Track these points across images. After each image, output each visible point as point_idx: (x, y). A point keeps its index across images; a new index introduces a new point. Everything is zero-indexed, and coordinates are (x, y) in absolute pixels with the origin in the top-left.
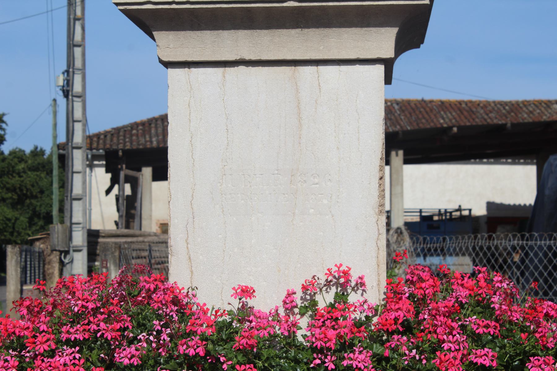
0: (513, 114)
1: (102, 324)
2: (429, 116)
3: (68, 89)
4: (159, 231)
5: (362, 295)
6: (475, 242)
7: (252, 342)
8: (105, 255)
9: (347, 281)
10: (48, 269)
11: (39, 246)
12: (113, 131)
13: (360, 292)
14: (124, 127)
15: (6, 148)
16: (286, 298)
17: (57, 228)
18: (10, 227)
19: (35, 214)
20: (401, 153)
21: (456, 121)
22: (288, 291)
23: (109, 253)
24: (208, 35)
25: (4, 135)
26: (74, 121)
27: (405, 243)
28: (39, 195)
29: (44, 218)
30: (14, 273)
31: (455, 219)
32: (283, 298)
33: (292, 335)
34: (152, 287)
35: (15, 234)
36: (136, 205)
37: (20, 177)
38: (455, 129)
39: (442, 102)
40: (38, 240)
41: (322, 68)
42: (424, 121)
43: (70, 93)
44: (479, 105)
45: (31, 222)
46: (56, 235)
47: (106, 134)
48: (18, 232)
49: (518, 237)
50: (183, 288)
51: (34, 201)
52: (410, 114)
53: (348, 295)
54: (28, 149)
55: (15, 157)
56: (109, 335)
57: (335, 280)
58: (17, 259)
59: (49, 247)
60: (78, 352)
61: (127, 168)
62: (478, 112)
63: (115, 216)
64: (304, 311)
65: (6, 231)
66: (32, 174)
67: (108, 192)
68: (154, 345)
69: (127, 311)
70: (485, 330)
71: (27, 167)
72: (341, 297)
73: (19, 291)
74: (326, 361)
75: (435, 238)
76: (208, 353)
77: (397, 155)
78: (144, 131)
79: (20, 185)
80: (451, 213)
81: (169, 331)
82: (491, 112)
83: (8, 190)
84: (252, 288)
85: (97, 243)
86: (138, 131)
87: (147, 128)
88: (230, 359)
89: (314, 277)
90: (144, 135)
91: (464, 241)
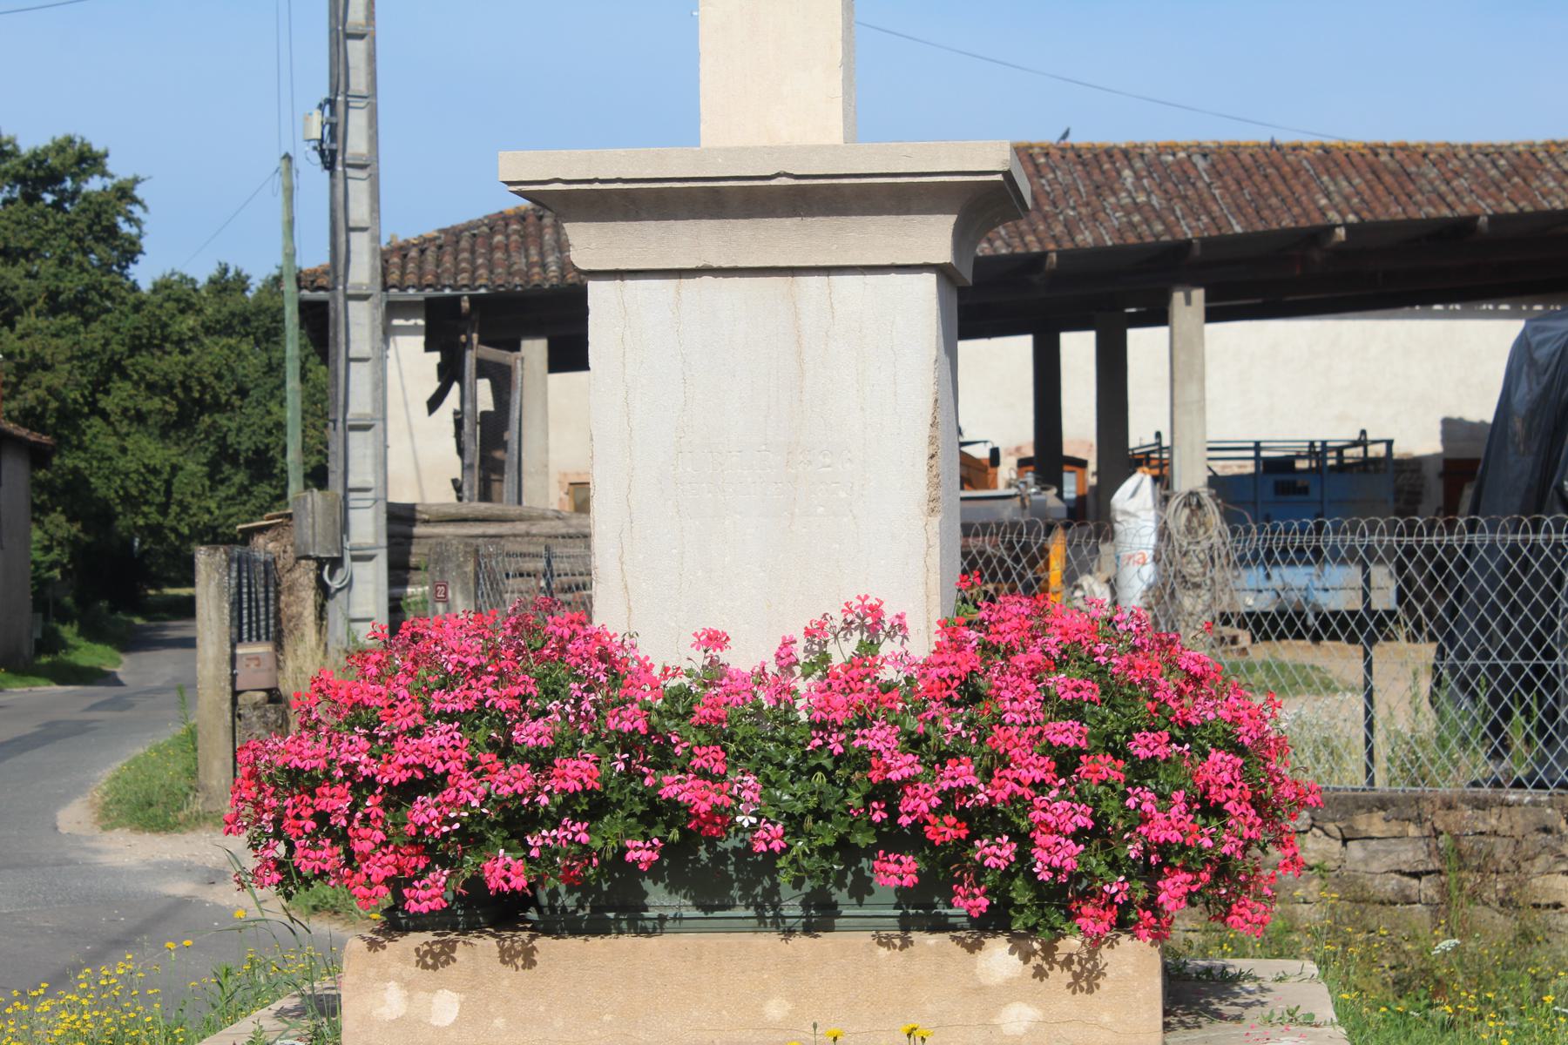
0: (1516, 179)
1: (490, 691)
2: (1290, 188)
3: (334, 146)
4: (568, 507)
5: (902, 643)
6: (1286, 540)
8: (442, 572)
9: (878, 621)
10: (287, 605)
11: (264, 546)
12: (443, 236)
13: (898, 639)
14: (470, 226)
15: (144, 274)
16: (781, 649)
17: (310, 505)
18: (157, 491)
19: (224, 455)
20: (1198, 295)
21: (1363, 200)
22: (784, 638)
24: (651, 228)
25: (140, 236)
26: (349, 230)
27: (1210, 532)
28: (236, 401)
30: (213, 615)
32: (776, 649)
34: (567, 633)
35: (174, 509)
36: (506, 436)
37: (185, 352)
38: (1341, 233)
39: (1326, 150)
40: (261, 530)
41: (836, 279)
42: (1274, 201)
43: (340, 158)
44: (1425, 155)
46: (310, 520)
47: (423, 246)
48: (180, 503)
49: (1440, 528)
50: (615, 635)
51: (221, 419)
52: (1239, 183)
53: (879, 644)
54: (202, 273)
55: (168, 298)
57: (858, 621)
58: (221, 579)
59: (289, 548)
60: (459, 730)
61: (482, 342)
62: (1424, 175)
63: (454, 467)
64: (809, 669)
65: (146, 502)
66: (217, 344)
67: (434, 403)
68: (572, 718)
70: (1074, 694)
71: (203, 325)
73: (227, 658)
74: (831, 741)
75: (1296, 525)
76: (652, 730)
77: (1188, 301)
78: (524, 236)
79: (184, 374)
80: (1340, 450)
82: (1457, 174)
84: (724, 634)
86: (508, 237)
87: (531, 229)
88: (687, 739)
89: (824, 615)
90: (524, 247)
91: (1262, 536)
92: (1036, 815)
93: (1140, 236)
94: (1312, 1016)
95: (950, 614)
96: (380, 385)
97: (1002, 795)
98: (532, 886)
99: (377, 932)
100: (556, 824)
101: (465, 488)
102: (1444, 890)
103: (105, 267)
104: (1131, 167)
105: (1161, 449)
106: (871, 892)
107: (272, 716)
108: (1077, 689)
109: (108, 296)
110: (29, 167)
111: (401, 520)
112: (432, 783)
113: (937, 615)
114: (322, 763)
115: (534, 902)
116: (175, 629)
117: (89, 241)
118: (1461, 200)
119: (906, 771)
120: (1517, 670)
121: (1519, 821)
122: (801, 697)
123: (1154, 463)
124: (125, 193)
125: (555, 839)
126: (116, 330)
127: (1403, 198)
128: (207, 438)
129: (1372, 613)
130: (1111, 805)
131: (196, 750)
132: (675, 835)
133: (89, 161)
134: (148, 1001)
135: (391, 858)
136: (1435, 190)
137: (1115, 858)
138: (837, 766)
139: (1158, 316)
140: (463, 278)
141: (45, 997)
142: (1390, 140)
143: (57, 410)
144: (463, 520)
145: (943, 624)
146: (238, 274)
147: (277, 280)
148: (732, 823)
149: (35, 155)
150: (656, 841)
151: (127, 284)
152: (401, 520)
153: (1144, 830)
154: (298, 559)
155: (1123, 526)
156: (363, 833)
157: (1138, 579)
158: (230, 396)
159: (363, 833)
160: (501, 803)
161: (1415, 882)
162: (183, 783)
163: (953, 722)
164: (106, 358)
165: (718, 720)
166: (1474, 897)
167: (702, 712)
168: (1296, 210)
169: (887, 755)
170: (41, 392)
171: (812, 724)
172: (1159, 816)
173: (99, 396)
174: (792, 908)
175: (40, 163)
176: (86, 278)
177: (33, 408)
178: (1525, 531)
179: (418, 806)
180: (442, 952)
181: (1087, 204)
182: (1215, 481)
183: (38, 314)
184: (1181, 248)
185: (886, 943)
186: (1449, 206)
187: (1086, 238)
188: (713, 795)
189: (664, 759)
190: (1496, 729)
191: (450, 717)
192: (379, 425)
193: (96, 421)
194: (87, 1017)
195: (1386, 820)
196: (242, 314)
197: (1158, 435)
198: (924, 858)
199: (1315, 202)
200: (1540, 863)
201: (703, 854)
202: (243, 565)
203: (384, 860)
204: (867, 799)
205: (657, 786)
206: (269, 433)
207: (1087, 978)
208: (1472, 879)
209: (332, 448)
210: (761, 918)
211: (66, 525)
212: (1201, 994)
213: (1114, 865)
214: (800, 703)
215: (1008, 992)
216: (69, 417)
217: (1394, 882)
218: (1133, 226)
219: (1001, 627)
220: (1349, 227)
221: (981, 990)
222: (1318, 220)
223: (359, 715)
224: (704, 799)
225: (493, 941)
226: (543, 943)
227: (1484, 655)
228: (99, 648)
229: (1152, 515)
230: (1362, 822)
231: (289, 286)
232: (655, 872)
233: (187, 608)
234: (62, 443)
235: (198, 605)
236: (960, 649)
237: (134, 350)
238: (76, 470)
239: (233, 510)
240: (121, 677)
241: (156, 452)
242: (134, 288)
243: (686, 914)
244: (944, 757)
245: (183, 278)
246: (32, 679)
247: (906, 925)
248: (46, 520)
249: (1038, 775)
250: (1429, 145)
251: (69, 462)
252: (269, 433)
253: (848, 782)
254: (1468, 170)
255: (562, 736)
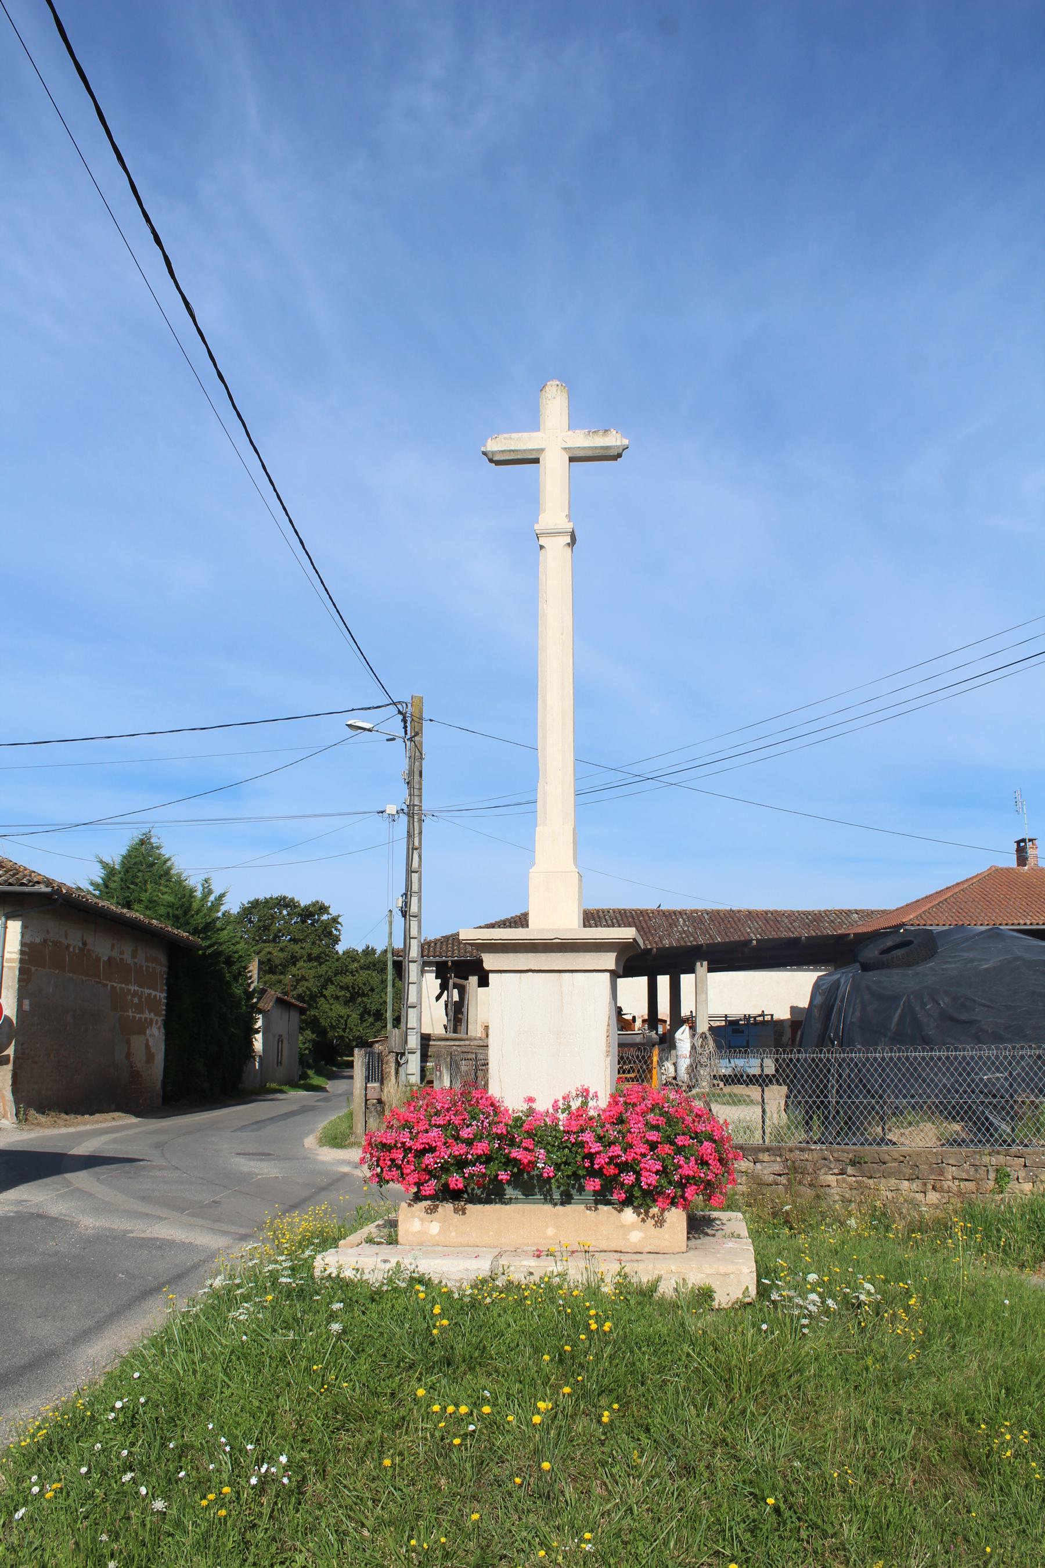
1: (452, 1117)
9: (588, 1094)
11: (378, 1048)
15: (340, 948)
19: (366, 1012)
20: (705, 963)
23: (441, 1059)
24: (511, 956)
26: (410, 938)
29: (374, 1014)
34: (480, 1097)
35: (348, 1030)
37: (353, 976)
38: (754, 942)
40: (377, 1042)
41: (575, 974)
42: (732, 930)
45: (362, 1020)
47: (436, 942)
51: (365, 999)
55: (348, 957)
56: (457, 1122)
62: (783, 921)
67: (438, 998)
69: (465, 1109)
76: (508, 1133)
77: (702, 966)
80: (755, 1018)
82: (795, 921)
83: (342, 988)
85: (428, 1045)
92: (642, 1165)
95: (614, 1091)
97: (630, 1158)
100: (474, 1165)
102: (789, 1180)
103: (327, 946)
105: (692, 1017)
106: (584, 1191)
107: (379, 1109)
108: (657, 1120)
109: (328, 955)
111: (425, 1039)
112: (432, 1149)
113: (609, 1092)
114: (393, 1141)
115: (466, 1191)
116: (347, 1072)
117: (322, 937)
118: (796, 930)
119: (597, 1149)
120: (814, 1102)
124: (335, 920)
129: (760, 1085)
130: (668, 1162)
132: (515, 1170)
133: (323, 909)
134: (332, 1219)
136: (787, 926)
139: (691, 970)
140: (449, 954)
142: (771, 909)
144: (447, 1040)
145: (611, 1095)
147: (386, 951)
148: (536, 1166)
149: (305, 907)
152: (425, 1039)
157: (684, 1063)
160: (455, 1157)
163: (613, 1131)
166: (800, 1183)
167: (526, 1126)
171: (564, 1131)
174: (556, 1196)
176: (321, 949)
182: (711, 1028)
183: (304, 961)
184: (699, 947)
185: (589, 1209)
187: (666, 943)
189: (512, 1143)
190: (807, 1123)
191: (439, 1126)
192: (419, 1006)
193: (322, 999)
197: (691, 1012)
200: (823, 1171)
201: (525, 1176)
202: (371, 1054)
204: (583, 1158)
205: (510, 1153)
207: (660, 1222)
208: (800, 1176)
210: (545, 1199)
213: (670, 1183)
215: (632, 1227)
216: (313, 997)
218: (683, 938)
221: (623, 1226)
222: (748, 938)
223: (407, 1125)
225: (451, 1205)
226: (469, 1206)
227: (803, 1097)
228: (321, 1078)
229: (689, 1041)
230: (761, 1156)
231: (389, 955)
232: (509, 1182)
233: (350, 1065)
234: (310, 1006)
236: (617, 1104)
241: (343, 1011)
242: (337, 953)
244: (611, 1144)
247: (597, 1202)
249: (643, 1151)
253: (577, 1152)
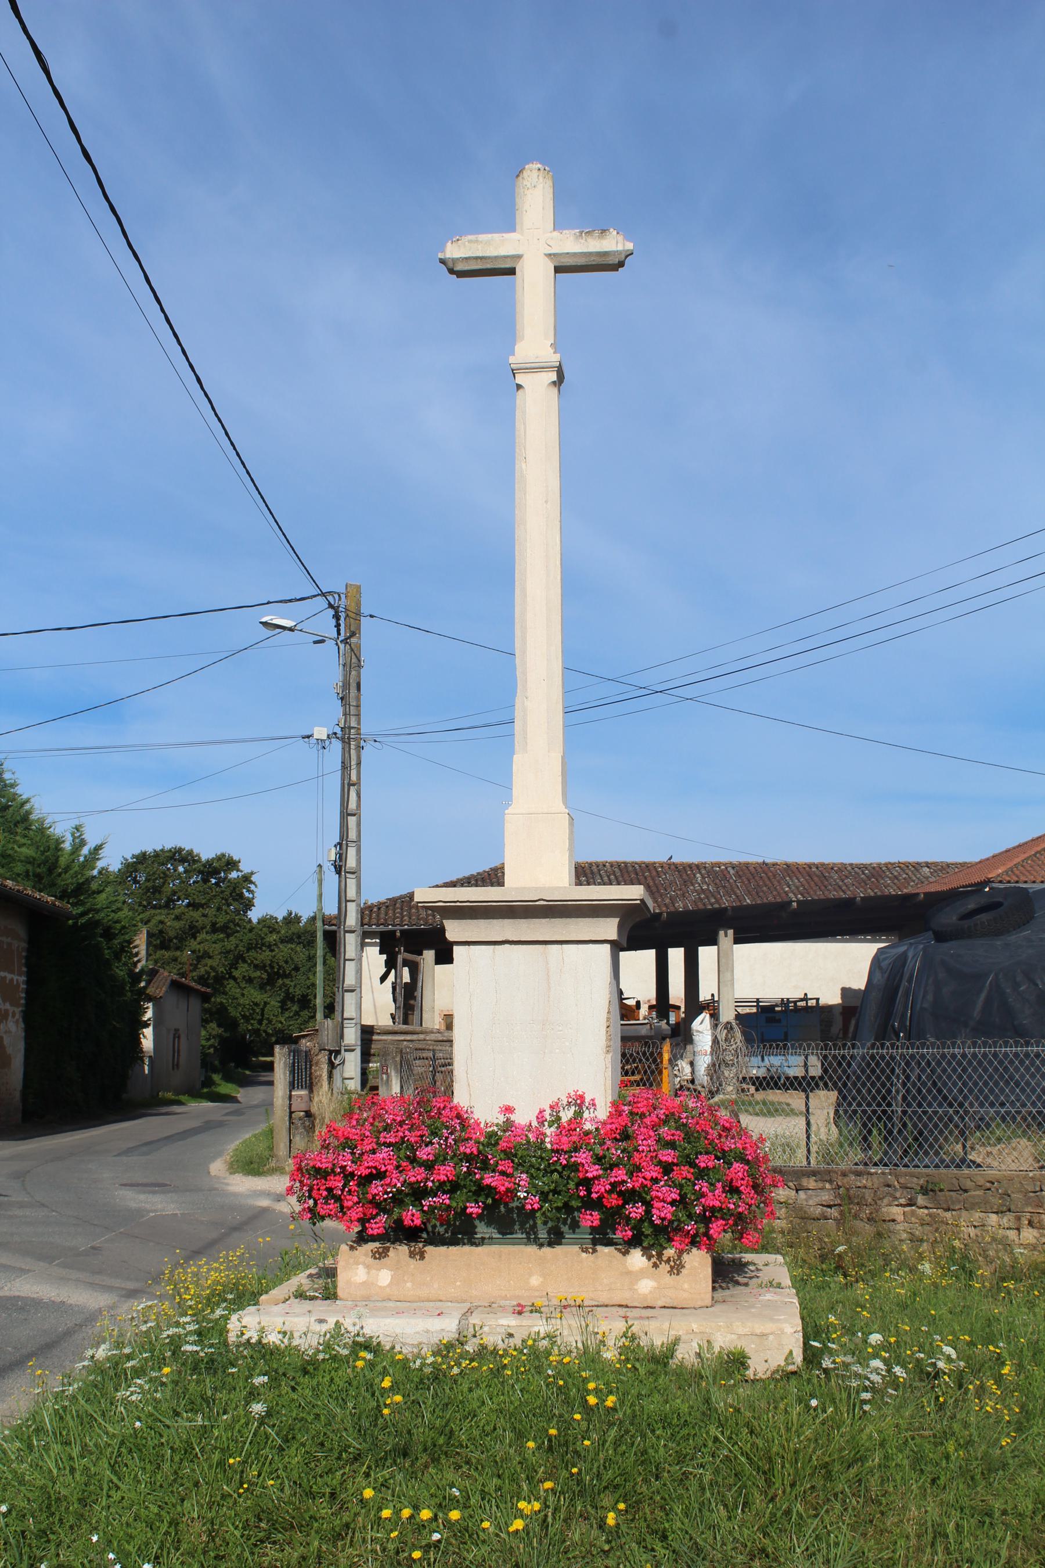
1: (407, 1133)
4: (443, 1028)
7: (510, 1145)
8: (385, 1060)
9: (583, 1102)
11: (305, 1044)
14: (401, 897)
19: (289, 997)
20: (731, 932)
21: (804, 888)
24: (482, 923)
25: (253, 899)
26: (347, 901)
30: (282, 1076)
31: (800, 1010)
32: (536, 1114)
33: (528, 1142)
34: (442, 1106)
35: (265, 1022)
36: (416, 994)
37: (272, 951)
38: (795, 904)
39: (788, 865)
40: (304, 1036)
41: (565, 946)
44: (832, 868)
47: (379, 906)
48: (268, 1019)
51: (287, 981)
55: (264, 926)
56: (413, 1139)
60: (392, 1151)
62: (832, 877)
63: (391, 1008)
65: (252, 1019)
67: (383, 979)
69: (424, 1122)
71: (280, 938)
72: (579, 1114)
76: (479, 1152)
77: (726, 936)
79: (271, 961)
80: (795, 1002)
81: (453, 1137)
82: (847, 877)
83: (256, 967)
85: (371, 1040)
88: (496, 1157)
92: (654, 1193)
93: (704, 904)
94: (780, 1284)
95: (616, 1097)
96: (359, 971)
97: (637, 1184)
98: (424, 1223)
99: (354, 1242)
101: (397, 1017)
102: (842, 1213)
103: (237, 912)
104: (700, 873)
105: (714, 1002)
106: (579, 1227)
107: (307, 1123)
108: (673, 1135)
110: (205, 867)
111: (367, 1032)
112: (380, 1175)
113: (610, 1099)
115: (426, 1230)
116: (264, 1077)
117: (230, 900)
118: (849, 888)
119: (595, 1173)
120: (874, 1112)
121: (876, 1182)
122: (548, 1136)
123: (711, 1008)
124: (247, 879)
125: (434, 1202)
126: (241, 941)
127: (823, 888)
128: (280, 990)
130: (687, 1189)
131: (272, 1138)
132: (489, 1201)
133: (231, 864)
135: (361, 1209)
136: (837, 884)
137: (690, 1213)
138: (563, 1169)
139: (713, 941)
140: (397, 921)
141: (204, 1265)
142: (816, 862)
143: (214, 976)
145: (613, 1103)
146: (296, 915)
147: (314, 918)
148: (516, 1195)
149: (208, 861)
150: (480, 1204)
151: (247, 920)
152: (367, 1032)
153: (703, 1200)
154: (320, 1050)
155: (696, 1038)
156: (348, 1197)
157: (704, 1062)
158: (291, 971)
159: (348, 1197)
160: (411, 1184)
161: (829, 1210)
162: (267, 1153)
163: (616, 1150)
164: (236, 953)
165: (509, 1148)
166: (856, 1216)
168: (775, 893)
169: (586, 1165)
170: (207, 968)
171: (553, 1150)
172: (710, 1194)
173: (233, 970)
174: (543, 1234)
175: (210, 865)
177: (204, 975)
178: (878, 1049)
179: (373, 1186)
180: (383, 1252)
181: (680, 890)
182: (738, 1016)
183: (207, 933)
184: (723, 911)
186: (843, 891)
187: (680, 906)
188: (506, 1183)
190: (865, 1139)
191: (389, 1145)
192: (358, 989)
193: (232, 982)
194: (222, 1275)
195: (816, 1181)
196: (298, 934)
197: (713, 995)
198: (603, 1213)
199: (783, 889)
200: (886, 1201)
201: (502, 1209)
202: (296, 1053)
203: (358, 1210)
204: (578, 1185)
205: (482, 1178)
206: (308, 988)
207: (677, 1268)
209: (337, 1000)
210: (528, 1238)
211: (217, 1029)
212: (732, 1272)
213: (690, 1216)
214: (547, 1140)
215: (641, 1274)
217: (819, 1209)
219: (639, 1105)
220: (798, 902)
221: (629, 1273)
222: (786, 899)
223: (347, 1144)
224: (503, 1185)
225: (406, 1247)
226: (429, 1249)
227: (859, 1105)
228: (230, 1085)
229: (710, 1032)
230: (805, 1182)
231: (319, 924)
232: (480, 1217)
233: (270, 1067)
234: (216, 992)
235: (275, 1065)
236: (621, 1115)
237: (248, 950)
238: (221, 1003)
239: (291, 1023)
240: (239, 1099)
241: (258, 996)
242: (250, 921)
243: (494, 1236)
244: (612, 1166)
245: (271, 916)
246: (199, 1100)
247: (595, 1242)
248: (208, 1026)
249: (655, 1175)
250: (834, 864)
251: (218, 1000)
252: (308, 988)
253: (569, 1177)
254: (852, 875)
255: (439, 1154)
